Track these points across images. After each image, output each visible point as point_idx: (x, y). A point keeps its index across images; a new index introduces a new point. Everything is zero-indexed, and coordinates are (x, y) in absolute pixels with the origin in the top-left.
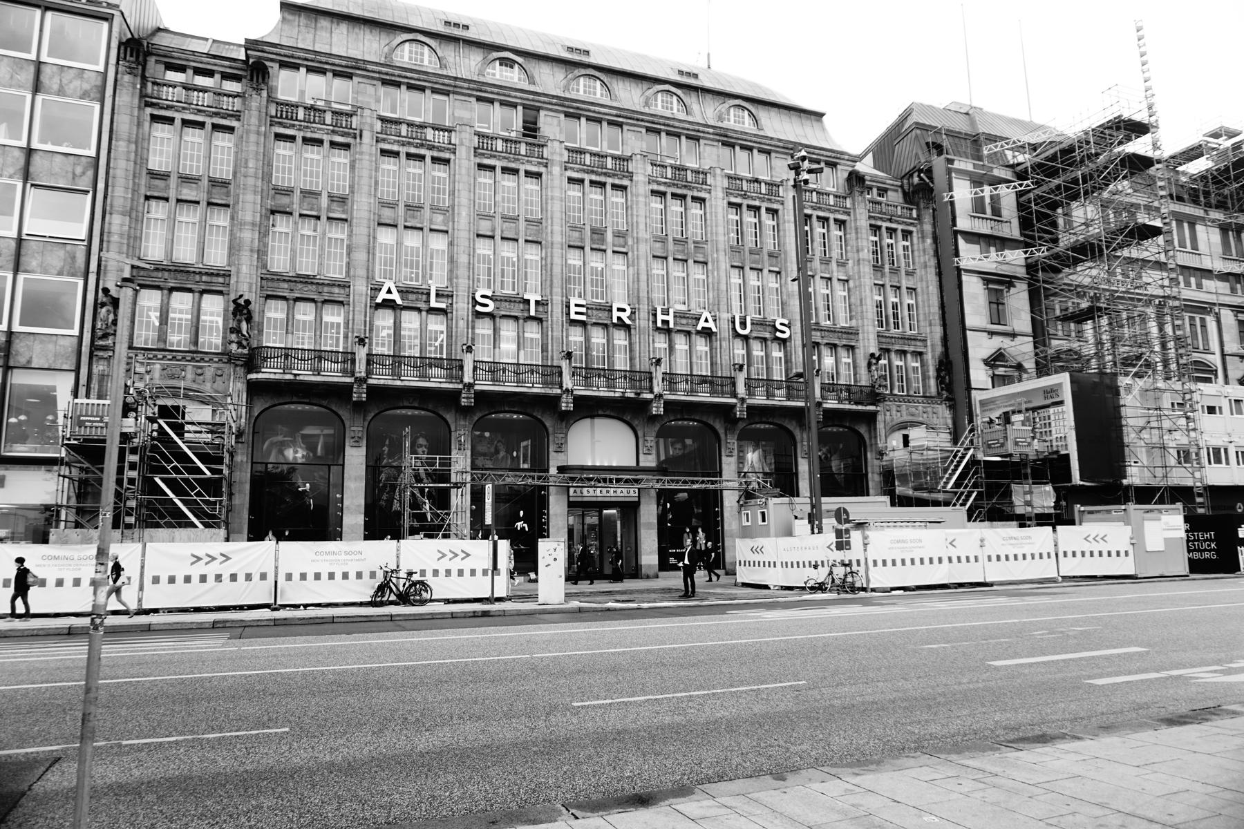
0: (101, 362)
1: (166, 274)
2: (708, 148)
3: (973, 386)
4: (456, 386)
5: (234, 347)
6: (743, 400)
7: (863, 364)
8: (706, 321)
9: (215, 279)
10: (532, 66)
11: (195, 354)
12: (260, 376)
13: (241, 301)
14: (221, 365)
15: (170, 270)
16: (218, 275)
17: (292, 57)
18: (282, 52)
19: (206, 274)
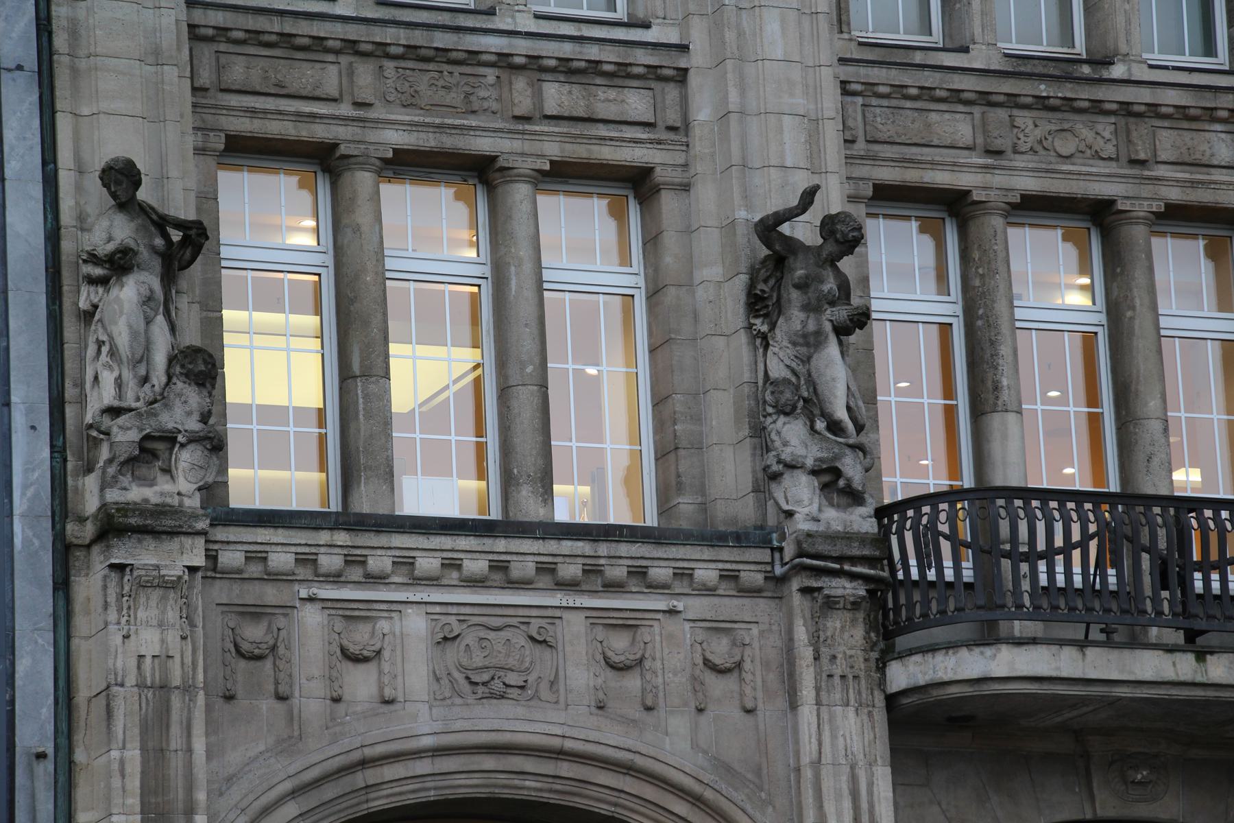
0: (148, 609)
1: (365, 73)
3: (335, 506)
5: (801, 494)
7: (718, 288)
9: (607, 101)
13: (804, 230)
14: (730, 607)
15: (381, 51)
16: (621, 75)
19: (567, 70)
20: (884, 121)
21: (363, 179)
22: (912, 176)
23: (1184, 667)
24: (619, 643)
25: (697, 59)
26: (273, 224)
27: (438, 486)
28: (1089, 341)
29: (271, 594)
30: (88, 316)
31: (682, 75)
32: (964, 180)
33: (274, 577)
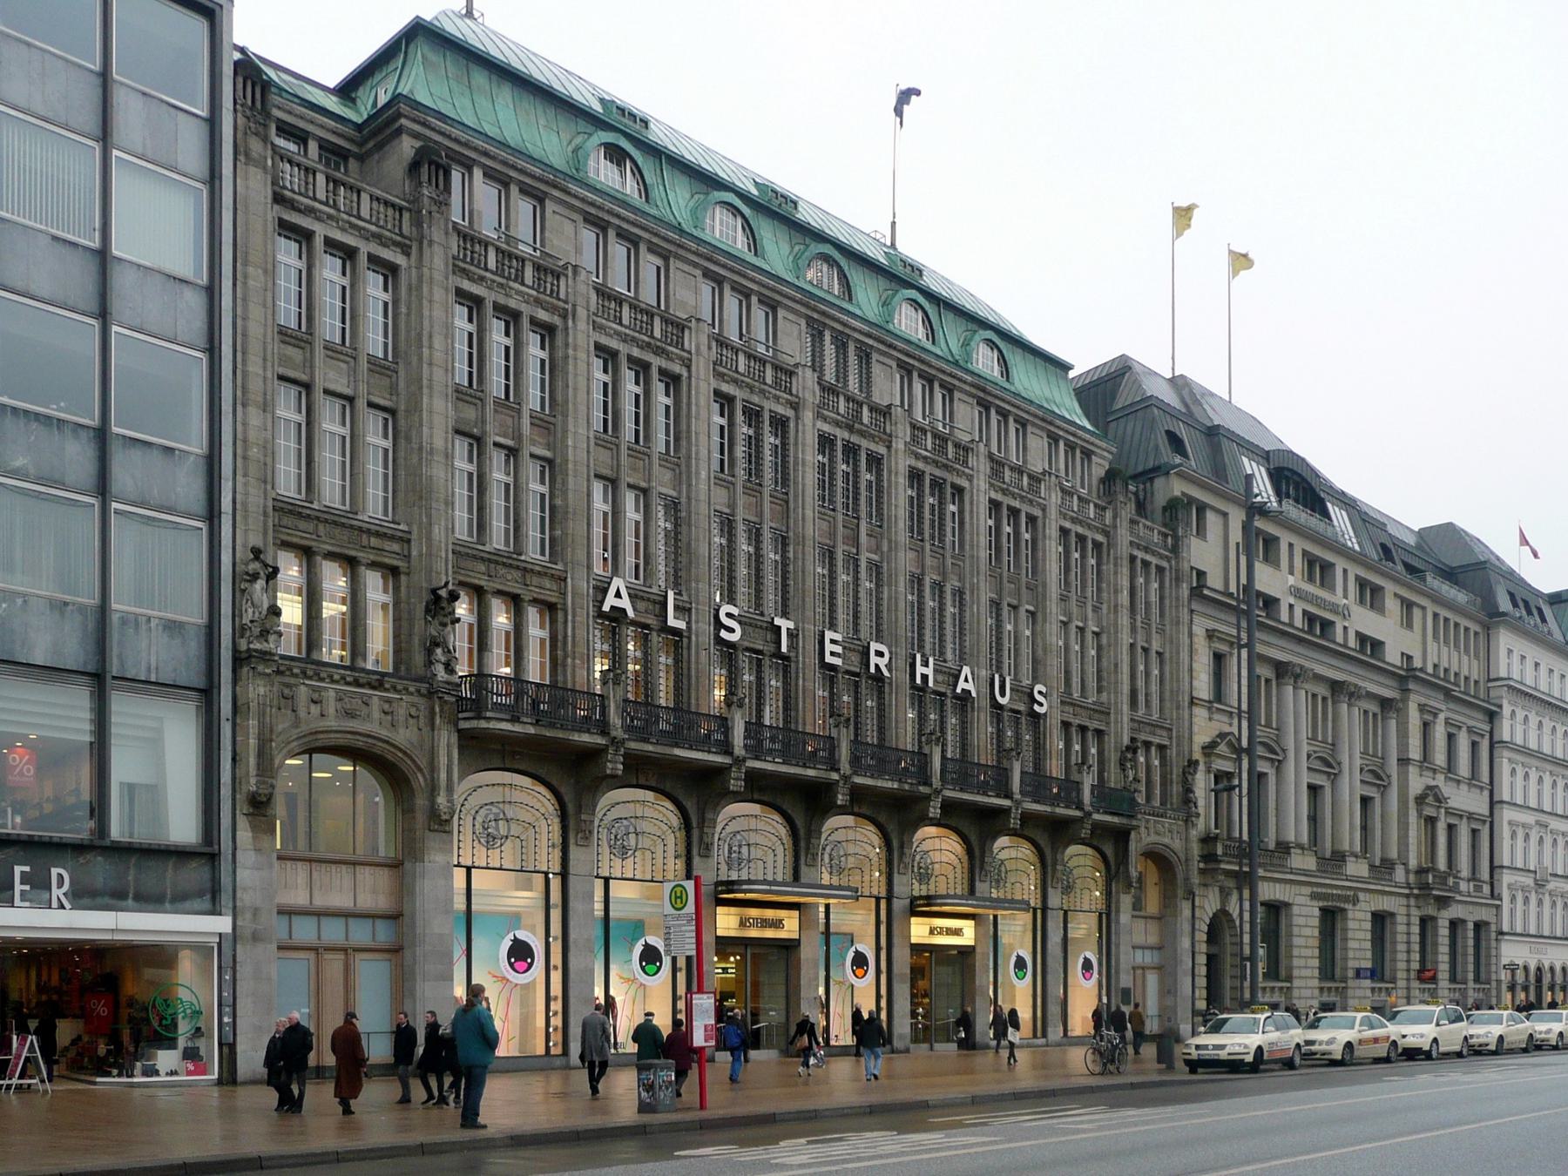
1: (321, 527)
2: (962, 406)
4: (719, 759)
5: (440, 671)
6: (739, 761)
7: (1113, 757)
8: (618, 595)
10: (857, 276)
11: (354, 673)
12: (483, 724)
13: (443, 593)
14: (416, 699)
17: (466, 145)
18: (455, 132)
19: (378, 534)
20: (286, 521)
21: (319, 558)
22: (468, 580)
23: (1048, 809)
24: (286, 691)
25: (414, 536)
26: (291, 570)
27: (333, 652)
28: (507, 633)
29: (292, 681)
30: (243, 591)
31: (409, 541)
32: (483, 583)
33: (293, 675)
